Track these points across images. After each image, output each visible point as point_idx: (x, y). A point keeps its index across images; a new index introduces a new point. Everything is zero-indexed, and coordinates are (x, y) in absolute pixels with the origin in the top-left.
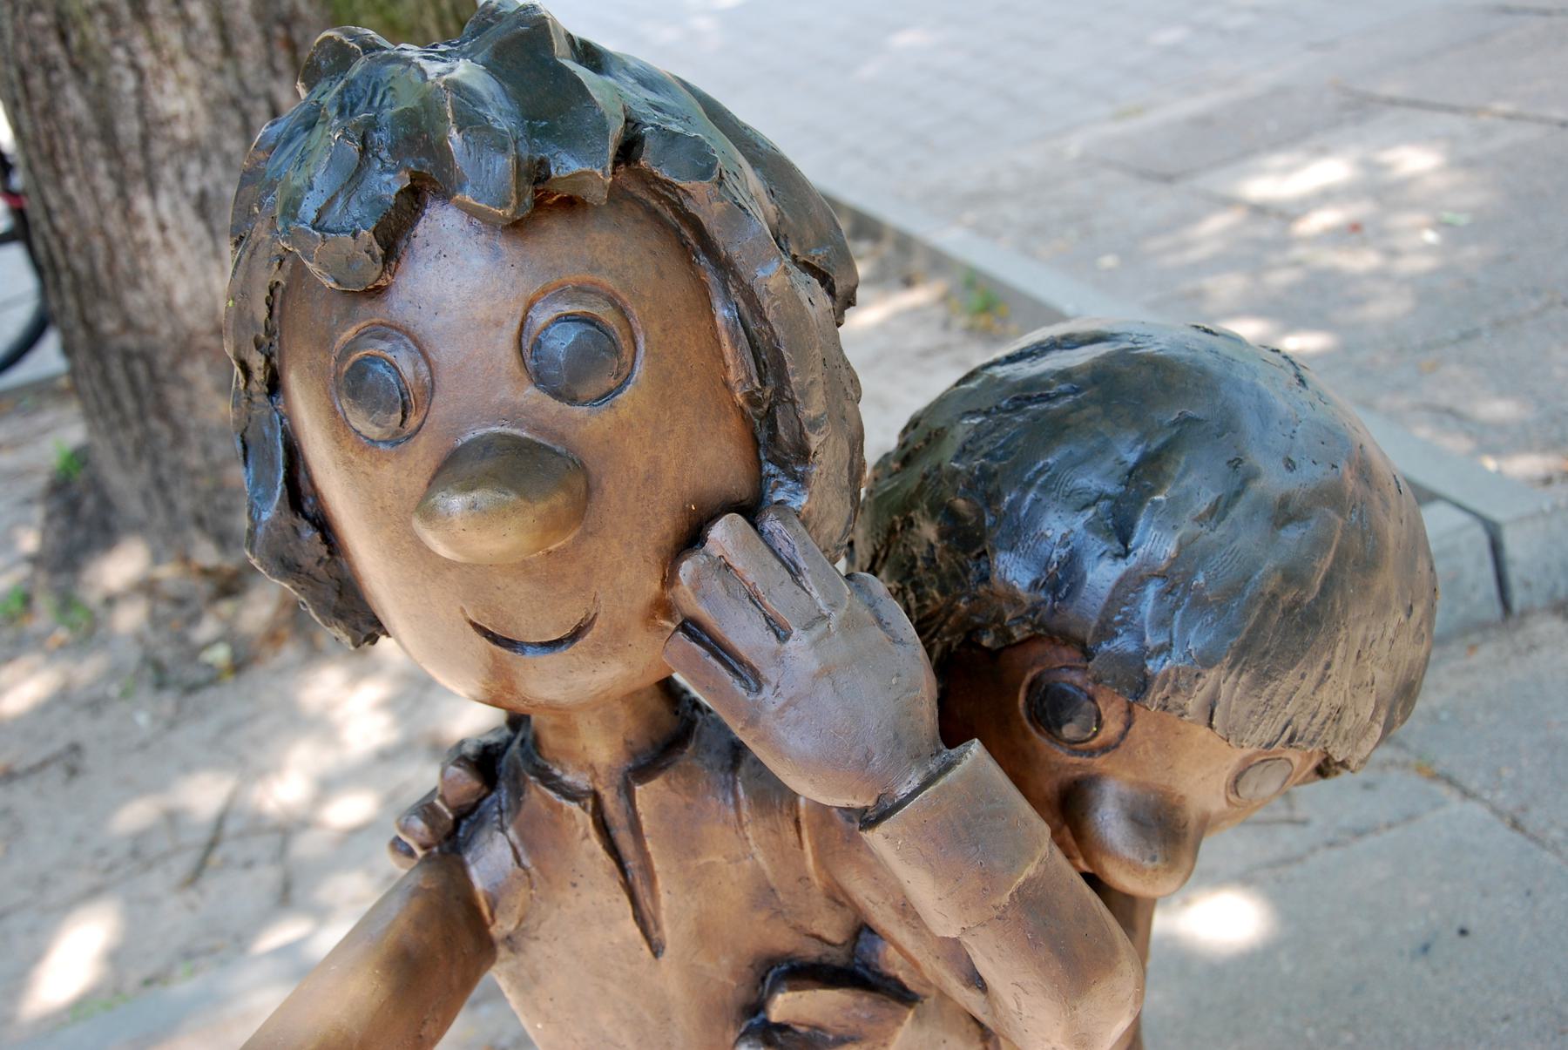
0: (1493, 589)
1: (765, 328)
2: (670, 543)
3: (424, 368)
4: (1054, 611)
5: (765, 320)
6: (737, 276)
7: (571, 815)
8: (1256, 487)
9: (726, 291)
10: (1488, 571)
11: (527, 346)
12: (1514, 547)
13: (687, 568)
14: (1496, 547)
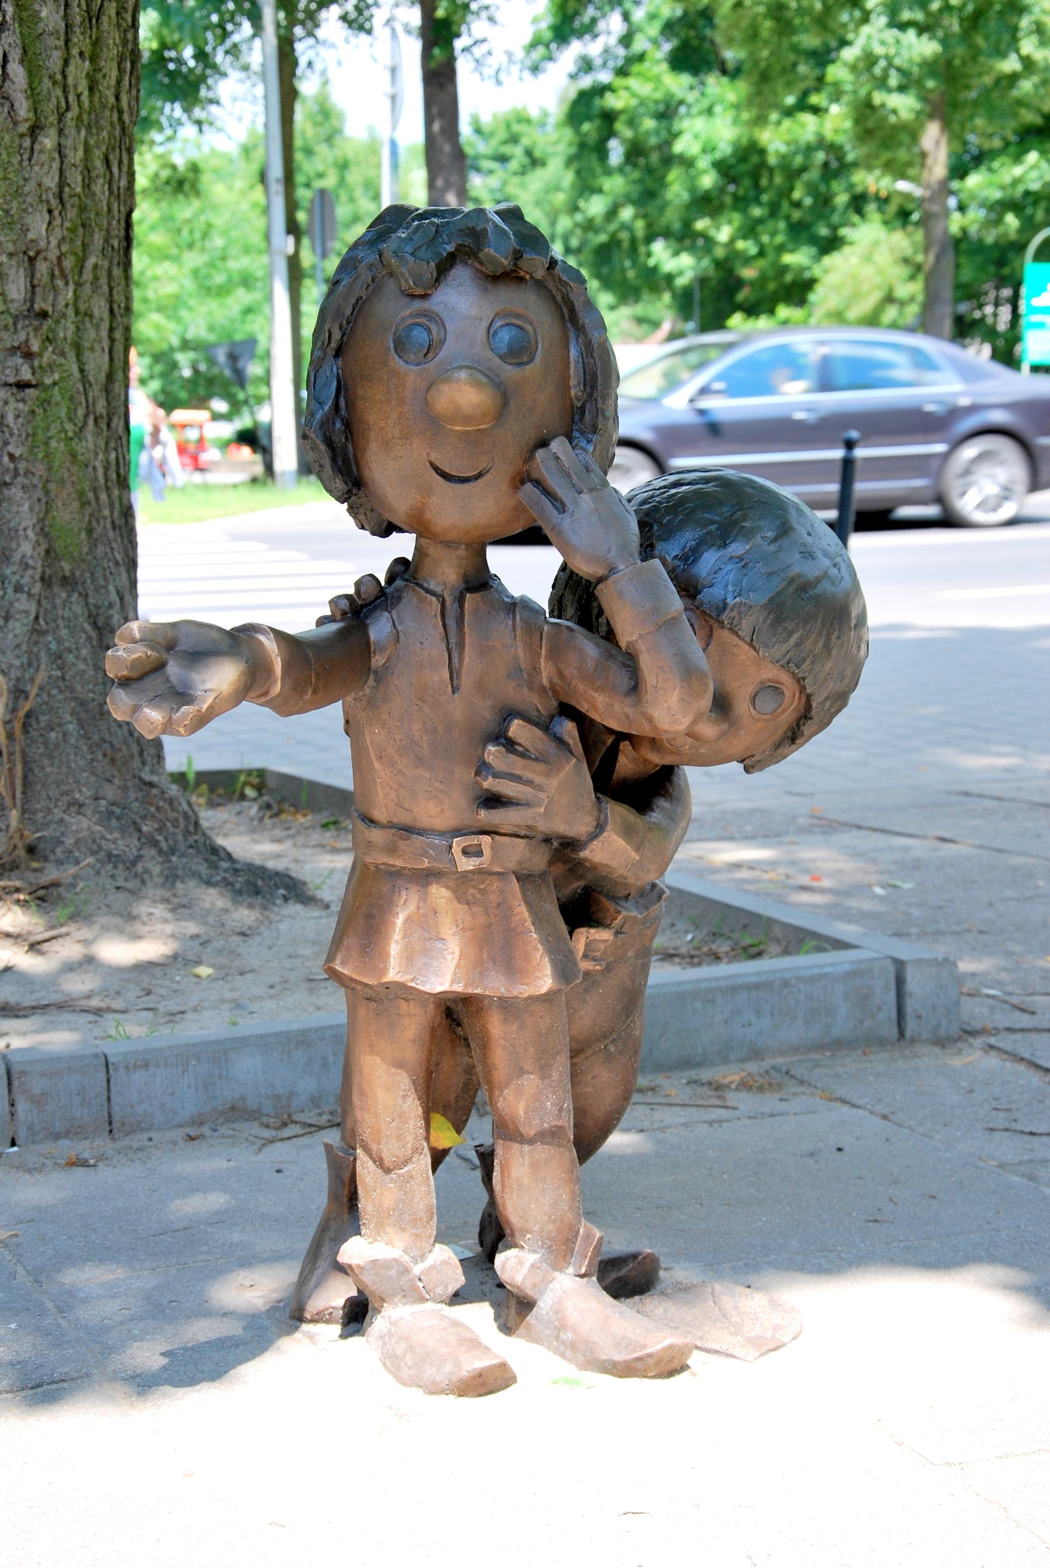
0: (894, 1014)
1: (592, 361)
2: (532, 443)
3: (442, 333)
4: (684, 570)
5: (592, 357)
6: (585, 334)
7: (430, 604)
8: (883, 20)
9: (577, 341)
10: (892, 996)
11: (492, 330)
12: (913, 984)
13: (540, 453)
14: (900, 981)
